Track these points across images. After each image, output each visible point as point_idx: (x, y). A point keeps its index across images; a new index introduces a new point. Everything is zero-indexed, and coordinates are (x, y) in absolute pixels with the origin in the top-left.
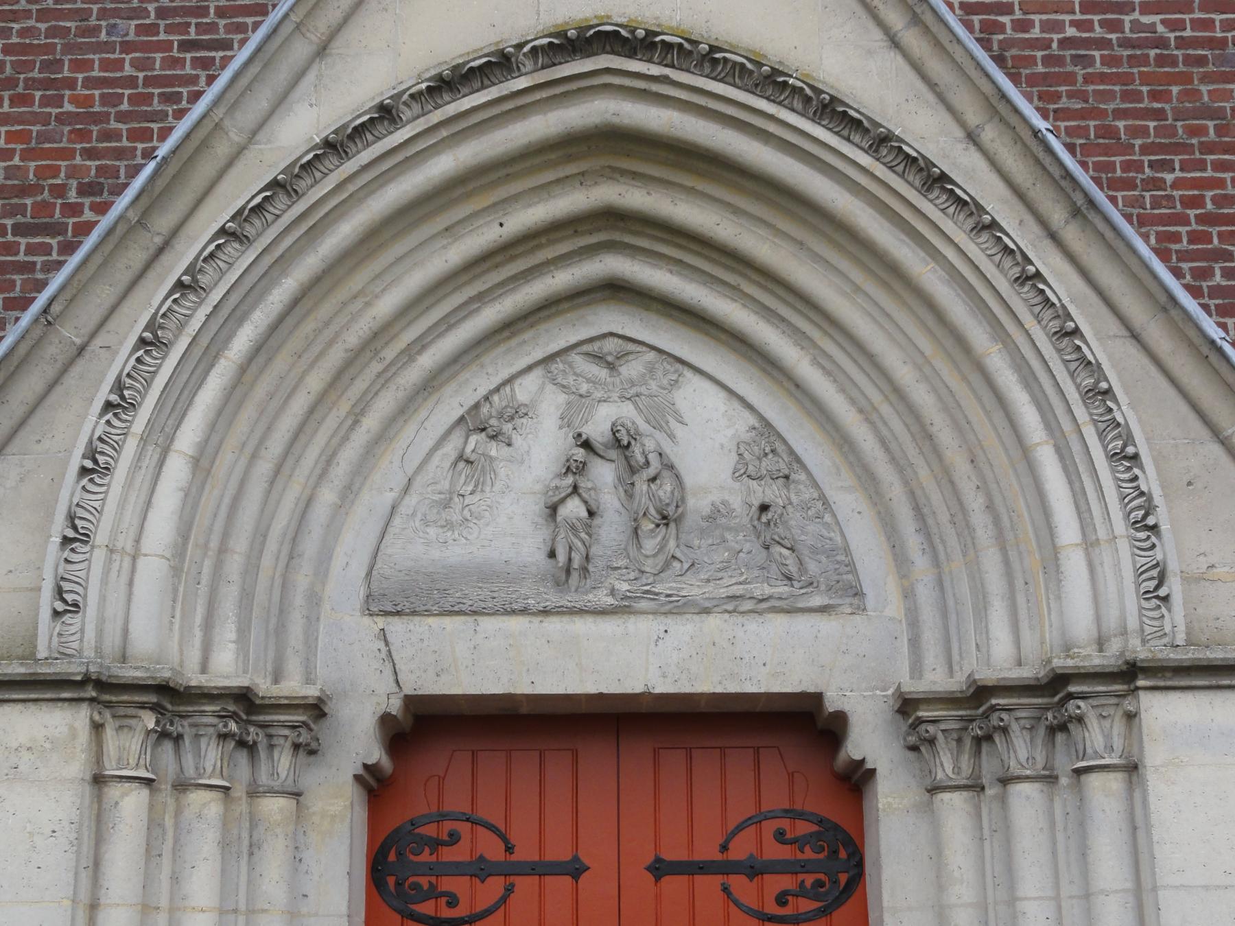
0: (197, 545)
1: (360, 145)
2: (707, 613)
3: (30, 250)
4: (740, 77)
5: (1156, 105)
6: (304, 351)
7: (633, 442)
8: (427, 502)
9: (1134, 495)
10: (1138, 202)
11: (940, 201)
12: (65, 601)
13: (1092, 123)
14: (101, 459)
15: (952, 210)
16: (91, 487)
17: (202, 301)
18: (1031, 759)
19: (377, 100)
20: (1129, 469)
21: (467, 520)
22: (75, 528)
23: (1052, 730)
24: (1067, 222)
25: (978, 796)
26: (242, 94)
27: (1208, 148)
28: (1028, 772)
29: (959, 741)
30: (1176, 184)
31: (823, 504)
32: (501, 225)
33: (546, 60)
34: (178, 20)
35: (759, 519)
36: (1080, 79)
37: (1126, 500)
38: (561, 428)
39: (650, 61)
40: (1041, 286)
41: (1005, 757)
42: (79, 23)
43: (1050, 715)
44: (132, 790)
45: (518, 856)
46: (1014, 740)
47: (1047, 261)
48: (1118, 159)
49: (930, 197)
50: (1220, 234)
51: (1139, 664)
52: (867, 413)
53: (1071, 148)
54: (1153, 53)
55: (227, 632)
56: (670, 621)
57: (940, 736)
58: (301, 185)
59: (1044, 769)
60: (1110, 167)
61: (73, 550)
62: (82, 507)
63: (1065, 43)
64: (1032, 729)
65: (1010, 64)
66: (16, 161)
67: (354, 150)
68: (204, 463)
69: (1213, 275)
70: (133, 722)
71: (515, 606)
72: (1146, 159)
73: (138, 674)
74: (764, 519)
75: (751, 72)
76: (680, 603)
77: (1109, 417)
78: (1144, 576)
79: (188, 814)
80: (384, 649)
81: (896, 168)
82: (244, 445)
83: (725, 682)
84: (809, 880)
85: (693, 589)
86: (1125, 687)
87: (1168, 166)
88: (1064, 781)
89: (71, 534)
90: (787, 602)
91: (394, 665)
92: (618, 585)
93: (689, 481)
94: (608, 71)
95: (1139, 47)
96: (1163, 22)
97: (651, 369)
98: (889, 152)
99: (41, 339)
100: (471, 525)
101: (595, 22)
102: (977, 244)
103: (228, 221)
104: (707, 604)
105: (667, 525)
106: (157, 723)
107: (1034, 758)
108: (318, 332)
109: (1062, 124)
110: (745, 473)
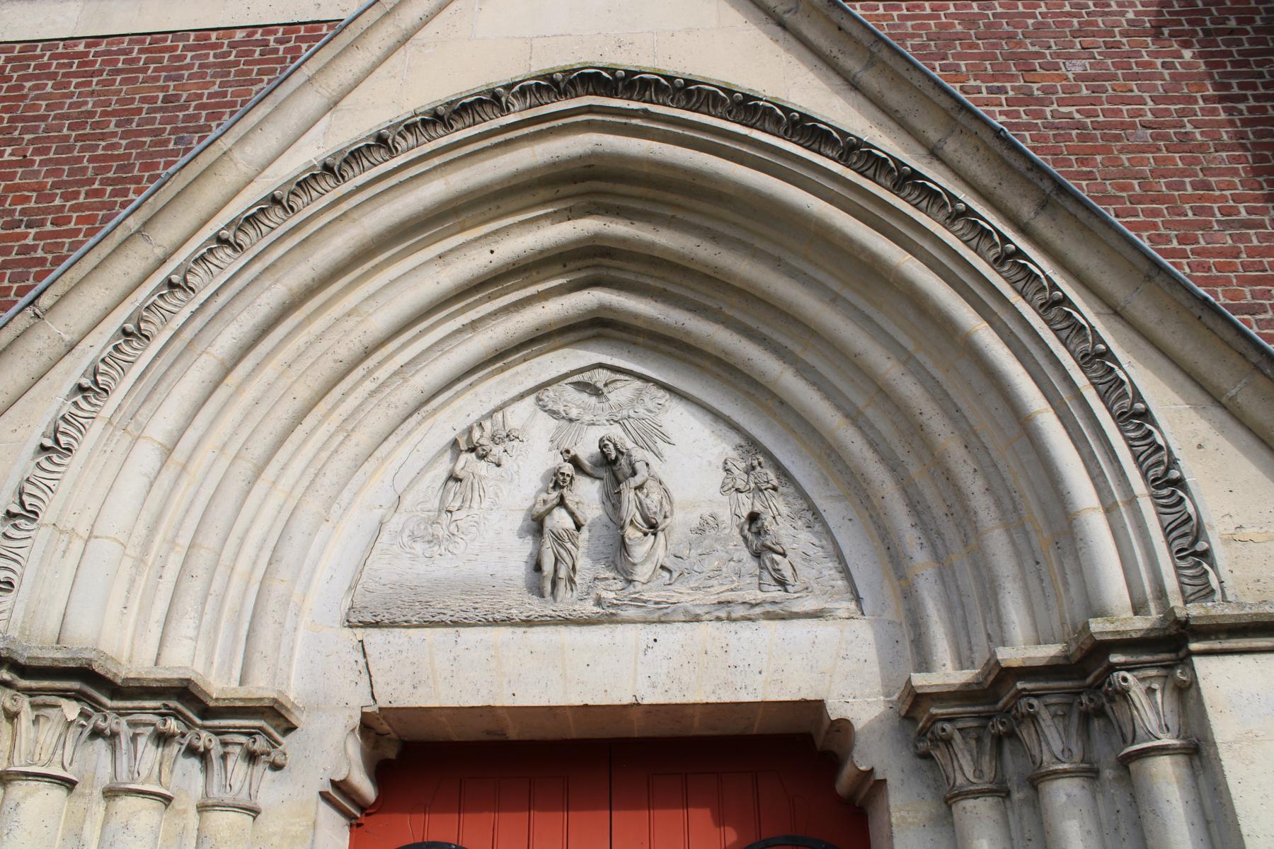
0: (165, 540)
1: (356, 169)
2: (698, 621)
4: (713, 107)
6: (294, 361)
7: (620, 457)
8: (415, 519)
9: (1149, 451)
11: (913, 196)
15: (924, 204)
16: (46, 465)
20: (1140, 426)
21: (453, 535)
22: (22, 504)
24: (1037, 214)
25: (1004, 802)
26: (253, 130)
27: (1135, 200)
28: (1066, 766)
29: (979, 740)
31: (813, 514)
32: (492, 252)
33: (534, 99)
35: (749, 530)
37: (1141, 459)
38: (550, 450)
39: (630, 99)
41: (1036, 752)
42: (154, 138)
43: (1084, 699)
44: (38, 790)
46: (1046, 731)
49: (902, 195)
51: (1192, 622)
52: (854, 417)
55: (185, 627)
56: (659, 628)
58: (297, 202)
59: (1082, 762)
61: (15, 526)
62: (34, 484)
67: (351, 173)
68: (179, 455)
71: (497, 616)
74: (754, 529)
75: (724, 100)
76: (669, 611)
77: (1110, 378)
78: (1174, 534)
80: (362, 661)
81: (867, 173)
82: (225, 445)
83: (718, 691)
85: (684, 595)
86: (1173, 656)
88: (1108, 773)
89: (16, 509)
90: (780, 606)
91: (370, 676)
92: (604, 594)
93: (676, 496)
94: (590, 109)
97: (639, 393)
98: (859, 159)
99: (25, 331)
100: (458, 540)
101: (579, 66)
102: (953, 232)
103: (223, 229)
104: (698, 611)
105: (655, 534)
107: (1070, 750)
108: (310, 344)
110: (733, 487)
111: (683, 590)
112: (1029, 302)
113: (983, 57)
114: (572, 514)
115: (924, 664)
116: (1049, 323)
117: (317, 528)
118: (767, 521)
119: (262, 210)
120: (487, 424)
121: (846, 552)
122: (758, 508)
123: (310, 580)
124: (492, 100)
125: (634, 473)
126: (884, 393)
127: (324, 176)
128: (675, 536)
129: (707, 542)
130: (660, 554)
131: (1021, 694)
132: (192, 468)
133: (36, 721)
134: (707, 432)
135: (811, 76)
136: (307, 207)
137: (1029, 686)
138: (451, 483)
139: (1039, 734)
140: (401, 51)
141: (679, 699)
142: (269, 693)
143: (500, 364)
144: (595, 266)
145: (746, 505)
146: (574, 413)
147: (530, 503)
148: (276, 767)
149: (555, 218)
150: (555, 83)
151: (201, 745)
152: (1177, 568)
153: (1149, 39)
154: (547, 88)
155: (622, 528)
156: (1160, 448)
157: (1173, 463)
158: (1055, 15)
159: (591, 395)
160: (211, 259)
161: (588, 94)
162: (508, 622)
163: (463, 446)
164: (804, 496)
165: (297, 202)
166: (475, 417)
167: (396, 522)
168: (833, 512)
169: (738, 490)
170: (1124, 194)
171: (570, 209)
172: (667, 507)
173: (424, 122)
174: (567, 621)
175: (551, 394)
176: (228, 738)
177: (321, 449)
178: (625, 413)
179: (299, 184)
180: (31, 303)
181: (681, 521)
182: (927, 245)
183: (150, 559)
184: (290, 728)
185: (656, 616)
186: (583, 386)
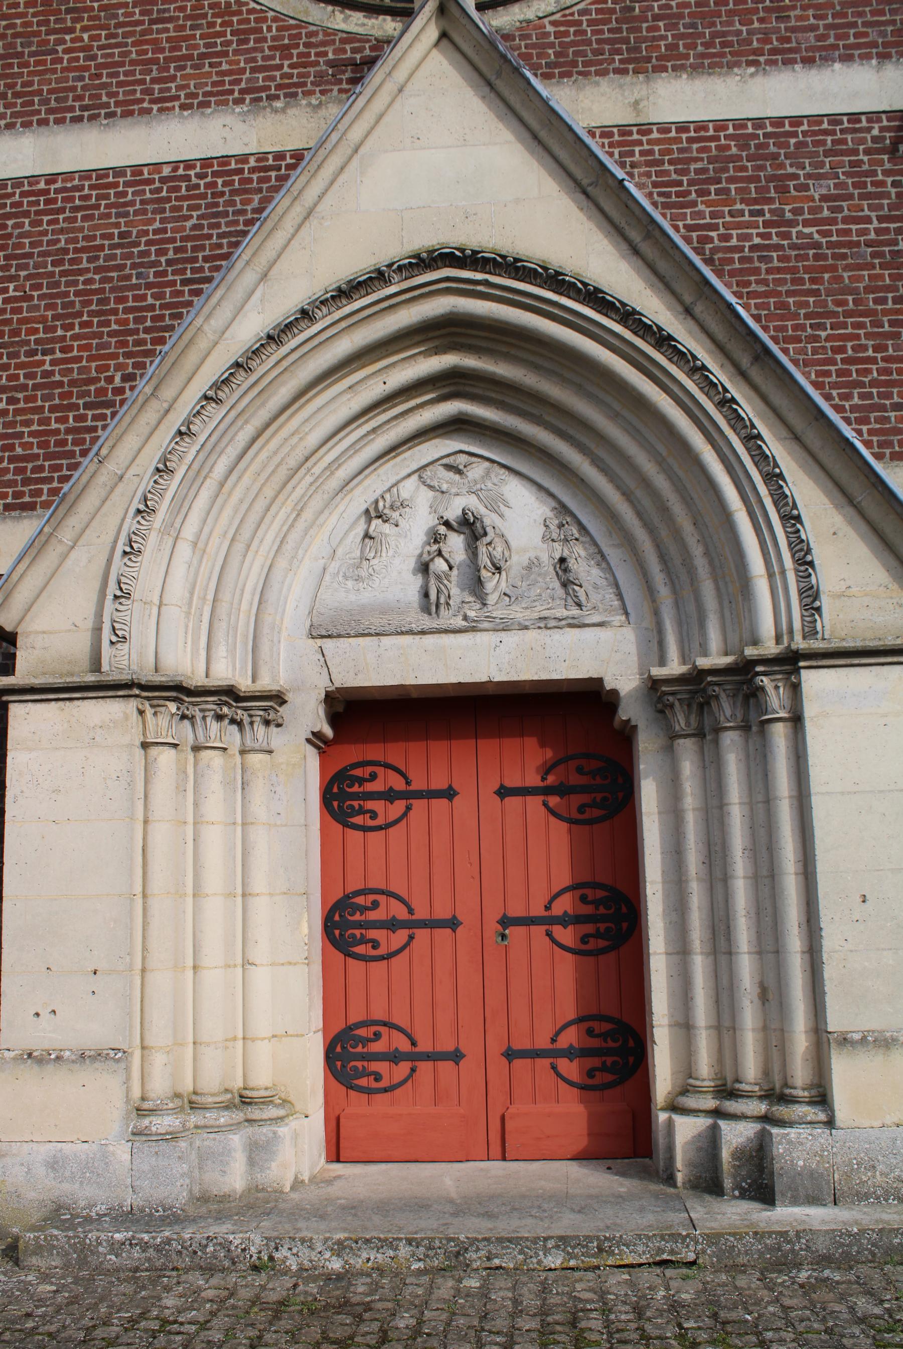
5: (814, 287)
10: (803, 351)
12: (117, 635)
13: (772, 300)
14: (135, 546)
15: (675, 359)
16: (129, 563)
17: (194, 442)
18: (733, 715)
19: (300, 306)
20: (794, 525)
22: (121, 589)
23: (747, 698)
24: (752, 364)
26: (214, 308)
27: (848, 314)
28: (731, 724)
29: (689, 706)
30: (827, 339)
34: (180, 266)
36: (763, 271)
39: (475, 270)
40: (735, 406)
43: (745, 687)
45: (414, 787)
48: (789, 323)
50: (857, 370)
52: (627, 495)
53: (757, 318)
54: (811, 252)
55: (221, 651)
56: (503, 634)
57: (677, 703)
58: (253, 364)
60: (784, 329)
63: (753, 248)
64: (734, 696)
65: (717, 263)
66: (84, 363)
68: (200, 545)
69: (853, 398)
70: (162, 709)
72: (808, 322)
73: (163, 679)
75: (541, 274)
79: (201, 764)
80: (322, 659)
84: (599, 796)
85: (518, 613)
93: (513, 544)
94: (448, 279)
95: (803, 249)
96: (818, 231)
97: (488, 473)
99: (95, 472)
104: (527, 623)
106: (178, 709)
108: (270, 458)
109: (752, 302)
111: (518, 609)
112: (738, 434)
113: (750, 179)
114: (447, 561)
115: (662, 662)
116: (748, 449)
117: (286, 577)
118: (571, 563)
119: (231, 374)
120: (387, 496)
121: (621, 583)
122: (566, 553)
123: (284, 611)
124: (379, 277)
125: (485, 534)
126: (645, 482)
127: (268, 343)
128: (513, 573)
129: (533, 577)
130: (503, 584)
131: (710, 684)
132: (208, 550)
133: (155, 714)
134: (533, 499)
135: (605, 242)
136: (261, 368)
137: (714, 679)
138: (367, 540)
139: (720, 706)
140: (307, 224)
141: (515, 678)
142: (275, 687)
143: (393, 454)
144: (455, 384)
145: (558, 551)
146: (445, 487)
147: (418, 552)
148: (279, 725)
149: (427, 354)
150: (422, 260)
151: (238, 718)
152: (802, 616)
153: (886, 157)
154: (417, 265)
155: (479, 571)
156: (802, 541)
157: (809, 551)
158: (815, 133)
159: (455, 473)
160: (203, 412)
161: (446, 266)
162: (410, 632)
163: (373, 514)
164: (595, 544)
165: (253, 364)
166: (379, 492)
167: (333, 567)
168: (614, 555)
169: (553, 540)
170: (840, 309)
171: (436, 347)
172: (507, 554)
173: (333, 297)
174: (446, 631)
175: (429, 473)
176: (252, 712)
177: (282, 525)
178: (478, 486)
179: (253, 352)
180: (97, 454)
181: (517, 561)
182: (676, 389)
183: (193, 611)
184: (283, 702)
185: (501, 627)
186: (448, 467)
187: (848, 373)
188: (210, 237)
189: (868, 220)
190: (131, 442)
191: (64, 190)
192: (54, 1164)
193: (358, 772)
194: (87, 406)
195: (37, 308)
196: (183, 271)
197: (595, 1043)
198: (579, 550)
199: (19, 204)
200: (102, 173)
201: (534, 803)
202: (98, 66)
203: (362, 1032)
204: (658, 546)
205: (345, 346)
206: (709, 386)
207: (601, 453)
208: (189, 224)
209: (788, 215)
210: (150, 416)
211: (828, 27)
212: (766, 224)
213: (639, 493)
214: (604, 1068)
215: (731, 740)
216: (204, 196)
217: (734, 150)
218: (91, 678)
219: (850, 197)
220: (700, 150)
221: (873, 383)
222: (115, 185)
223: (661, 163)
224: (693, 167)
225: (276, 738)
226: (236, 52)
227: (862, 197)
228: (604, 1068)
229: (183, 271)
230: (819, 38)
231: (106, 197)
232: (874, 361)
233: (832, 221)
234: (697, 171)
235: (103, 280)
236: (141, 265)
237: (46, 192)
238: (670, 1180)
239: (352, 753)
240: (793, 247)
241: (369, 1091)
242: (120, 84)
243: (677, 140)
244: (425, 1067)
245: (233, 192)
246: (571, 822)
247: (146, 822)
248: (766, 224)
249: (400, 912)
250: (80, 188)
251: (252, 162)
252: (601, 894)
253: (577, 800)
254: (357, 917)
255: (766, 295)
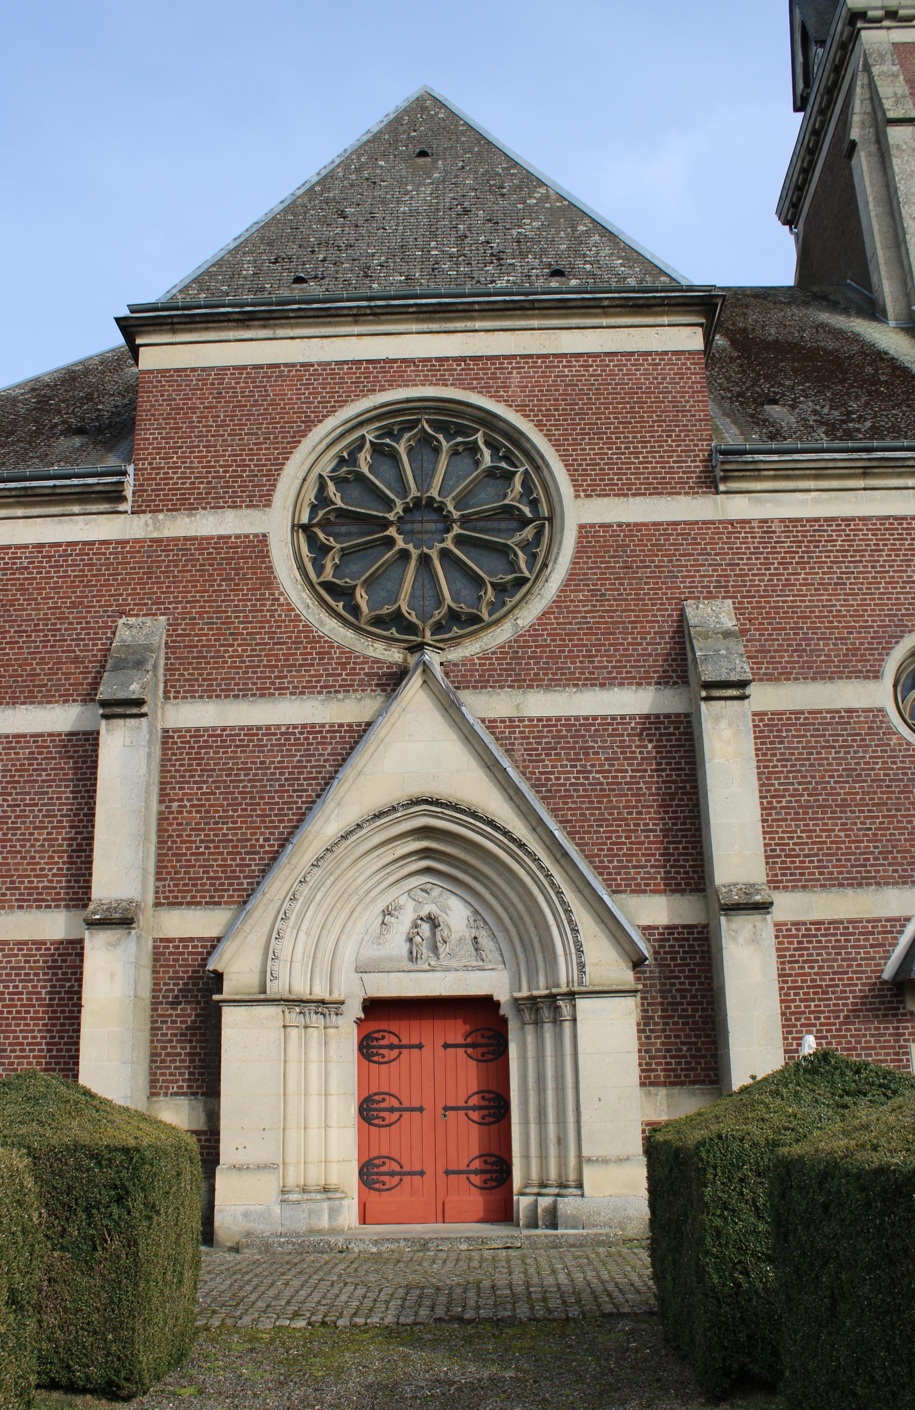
3: (250, 859)
27: (614, 820)
30: (604, 832)
45: (403, 1043)
47: (554, 870)
55: (317, 981)
63: (571, 784)
85: (454, 963)
87: (601, 826)
93: (453, 929)
115: (520, 991)
118: (480, 940)
124: (394, 809)
136: (339, 850)
145: (474, 933)
158: (604, 724)
162: (404, 971)
168: (500, 936)
181: (454, 937)
186: (422, 890)
187: (612, 850)
188: (306, 767)
189: (626, 771)
190: (277, 884)
191: (230, 735)
192: (246, 1215)
193: (376, 1035)
194: (246, 853)
195: (218, 799)
196: (293, 785)
197: (488, 1167)
198: (483, 933)
199: (207, 741)
200: (250, 728)
201: (461, 1051)
202: (247, 667)
203: (377, 1162)
204: (519, 934)
205: (376, 840)
206: (542, 868)
207: (494, 889)
208: (295, 759)
209: (589, 768)
210: (286, 872)
211: (613, 667)
212: (578, 772)
213: (511, 909)
214: (491, 1179)
215: (548, 1028)
216: (302, 744)
217: (564, 733)
218: (262, 997)
219: (619, 759)
220: (548, 732)
221: (624, 855)
222: (257, 735)
223: (528, 738)
224: (544, 740)
225: (340, 1020)
226: (318, 664)
227: (625, 759)
228: (491, 1179)
229: (293, 785)
230: (609, 673)
231: (253, 741)
232: (625, 843)
233: (609, 771)
234: (546, 743)
235: (252, 787)
236: (272, 780)
237: (221, 736)
238: (518, 1225)
239: (373, 1026)
240: (590, 784)
241: (380, 1190)
242: (258, 678)
243: (536, 726)
244: (407, 1179)
245: (318, 743)
246: (478, 1060)
247: (285, 1061)
248: (578, 772)
249: (396, 1103)
250: (239, 735)
251: (327, 728)
252: (491, 1095)
253: (481, 1050)
254: (375, 1106)
255: (576, 809)
